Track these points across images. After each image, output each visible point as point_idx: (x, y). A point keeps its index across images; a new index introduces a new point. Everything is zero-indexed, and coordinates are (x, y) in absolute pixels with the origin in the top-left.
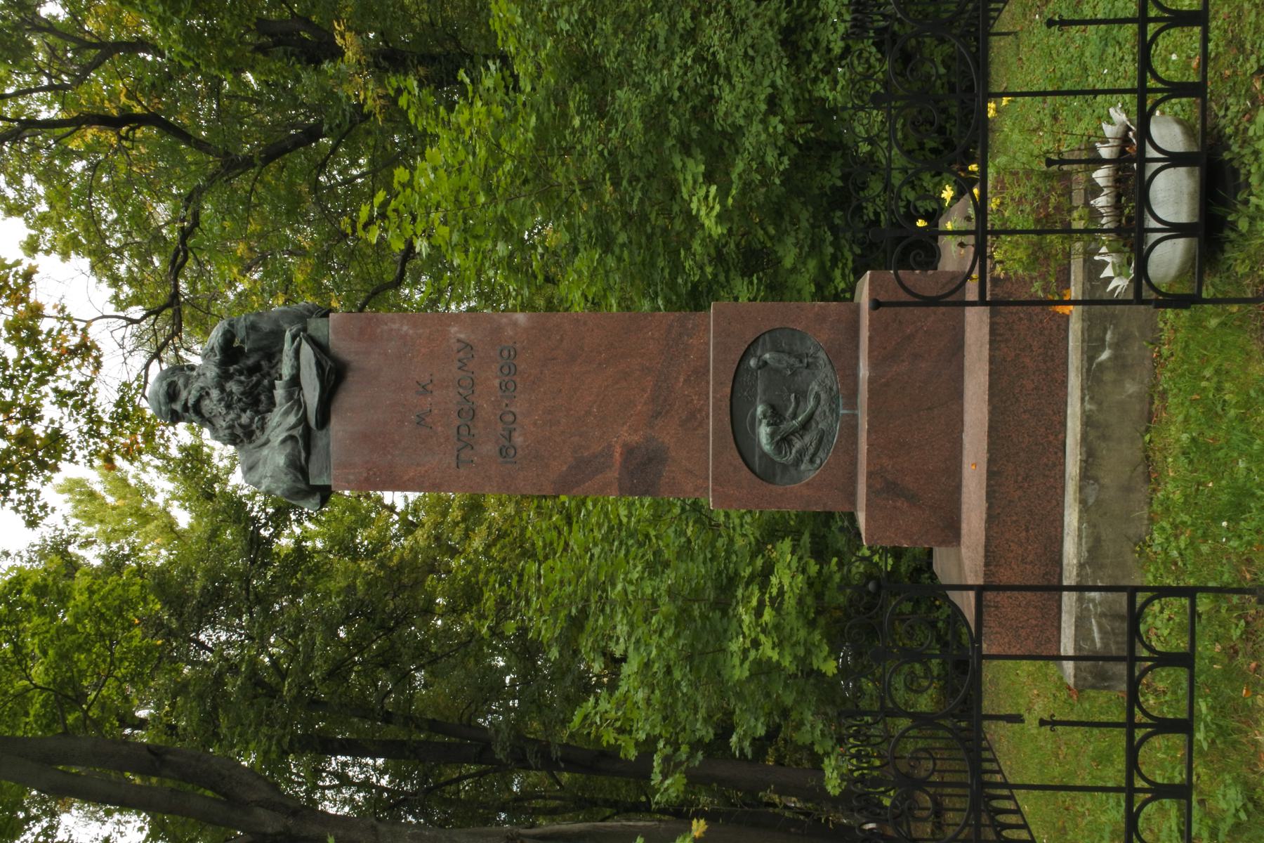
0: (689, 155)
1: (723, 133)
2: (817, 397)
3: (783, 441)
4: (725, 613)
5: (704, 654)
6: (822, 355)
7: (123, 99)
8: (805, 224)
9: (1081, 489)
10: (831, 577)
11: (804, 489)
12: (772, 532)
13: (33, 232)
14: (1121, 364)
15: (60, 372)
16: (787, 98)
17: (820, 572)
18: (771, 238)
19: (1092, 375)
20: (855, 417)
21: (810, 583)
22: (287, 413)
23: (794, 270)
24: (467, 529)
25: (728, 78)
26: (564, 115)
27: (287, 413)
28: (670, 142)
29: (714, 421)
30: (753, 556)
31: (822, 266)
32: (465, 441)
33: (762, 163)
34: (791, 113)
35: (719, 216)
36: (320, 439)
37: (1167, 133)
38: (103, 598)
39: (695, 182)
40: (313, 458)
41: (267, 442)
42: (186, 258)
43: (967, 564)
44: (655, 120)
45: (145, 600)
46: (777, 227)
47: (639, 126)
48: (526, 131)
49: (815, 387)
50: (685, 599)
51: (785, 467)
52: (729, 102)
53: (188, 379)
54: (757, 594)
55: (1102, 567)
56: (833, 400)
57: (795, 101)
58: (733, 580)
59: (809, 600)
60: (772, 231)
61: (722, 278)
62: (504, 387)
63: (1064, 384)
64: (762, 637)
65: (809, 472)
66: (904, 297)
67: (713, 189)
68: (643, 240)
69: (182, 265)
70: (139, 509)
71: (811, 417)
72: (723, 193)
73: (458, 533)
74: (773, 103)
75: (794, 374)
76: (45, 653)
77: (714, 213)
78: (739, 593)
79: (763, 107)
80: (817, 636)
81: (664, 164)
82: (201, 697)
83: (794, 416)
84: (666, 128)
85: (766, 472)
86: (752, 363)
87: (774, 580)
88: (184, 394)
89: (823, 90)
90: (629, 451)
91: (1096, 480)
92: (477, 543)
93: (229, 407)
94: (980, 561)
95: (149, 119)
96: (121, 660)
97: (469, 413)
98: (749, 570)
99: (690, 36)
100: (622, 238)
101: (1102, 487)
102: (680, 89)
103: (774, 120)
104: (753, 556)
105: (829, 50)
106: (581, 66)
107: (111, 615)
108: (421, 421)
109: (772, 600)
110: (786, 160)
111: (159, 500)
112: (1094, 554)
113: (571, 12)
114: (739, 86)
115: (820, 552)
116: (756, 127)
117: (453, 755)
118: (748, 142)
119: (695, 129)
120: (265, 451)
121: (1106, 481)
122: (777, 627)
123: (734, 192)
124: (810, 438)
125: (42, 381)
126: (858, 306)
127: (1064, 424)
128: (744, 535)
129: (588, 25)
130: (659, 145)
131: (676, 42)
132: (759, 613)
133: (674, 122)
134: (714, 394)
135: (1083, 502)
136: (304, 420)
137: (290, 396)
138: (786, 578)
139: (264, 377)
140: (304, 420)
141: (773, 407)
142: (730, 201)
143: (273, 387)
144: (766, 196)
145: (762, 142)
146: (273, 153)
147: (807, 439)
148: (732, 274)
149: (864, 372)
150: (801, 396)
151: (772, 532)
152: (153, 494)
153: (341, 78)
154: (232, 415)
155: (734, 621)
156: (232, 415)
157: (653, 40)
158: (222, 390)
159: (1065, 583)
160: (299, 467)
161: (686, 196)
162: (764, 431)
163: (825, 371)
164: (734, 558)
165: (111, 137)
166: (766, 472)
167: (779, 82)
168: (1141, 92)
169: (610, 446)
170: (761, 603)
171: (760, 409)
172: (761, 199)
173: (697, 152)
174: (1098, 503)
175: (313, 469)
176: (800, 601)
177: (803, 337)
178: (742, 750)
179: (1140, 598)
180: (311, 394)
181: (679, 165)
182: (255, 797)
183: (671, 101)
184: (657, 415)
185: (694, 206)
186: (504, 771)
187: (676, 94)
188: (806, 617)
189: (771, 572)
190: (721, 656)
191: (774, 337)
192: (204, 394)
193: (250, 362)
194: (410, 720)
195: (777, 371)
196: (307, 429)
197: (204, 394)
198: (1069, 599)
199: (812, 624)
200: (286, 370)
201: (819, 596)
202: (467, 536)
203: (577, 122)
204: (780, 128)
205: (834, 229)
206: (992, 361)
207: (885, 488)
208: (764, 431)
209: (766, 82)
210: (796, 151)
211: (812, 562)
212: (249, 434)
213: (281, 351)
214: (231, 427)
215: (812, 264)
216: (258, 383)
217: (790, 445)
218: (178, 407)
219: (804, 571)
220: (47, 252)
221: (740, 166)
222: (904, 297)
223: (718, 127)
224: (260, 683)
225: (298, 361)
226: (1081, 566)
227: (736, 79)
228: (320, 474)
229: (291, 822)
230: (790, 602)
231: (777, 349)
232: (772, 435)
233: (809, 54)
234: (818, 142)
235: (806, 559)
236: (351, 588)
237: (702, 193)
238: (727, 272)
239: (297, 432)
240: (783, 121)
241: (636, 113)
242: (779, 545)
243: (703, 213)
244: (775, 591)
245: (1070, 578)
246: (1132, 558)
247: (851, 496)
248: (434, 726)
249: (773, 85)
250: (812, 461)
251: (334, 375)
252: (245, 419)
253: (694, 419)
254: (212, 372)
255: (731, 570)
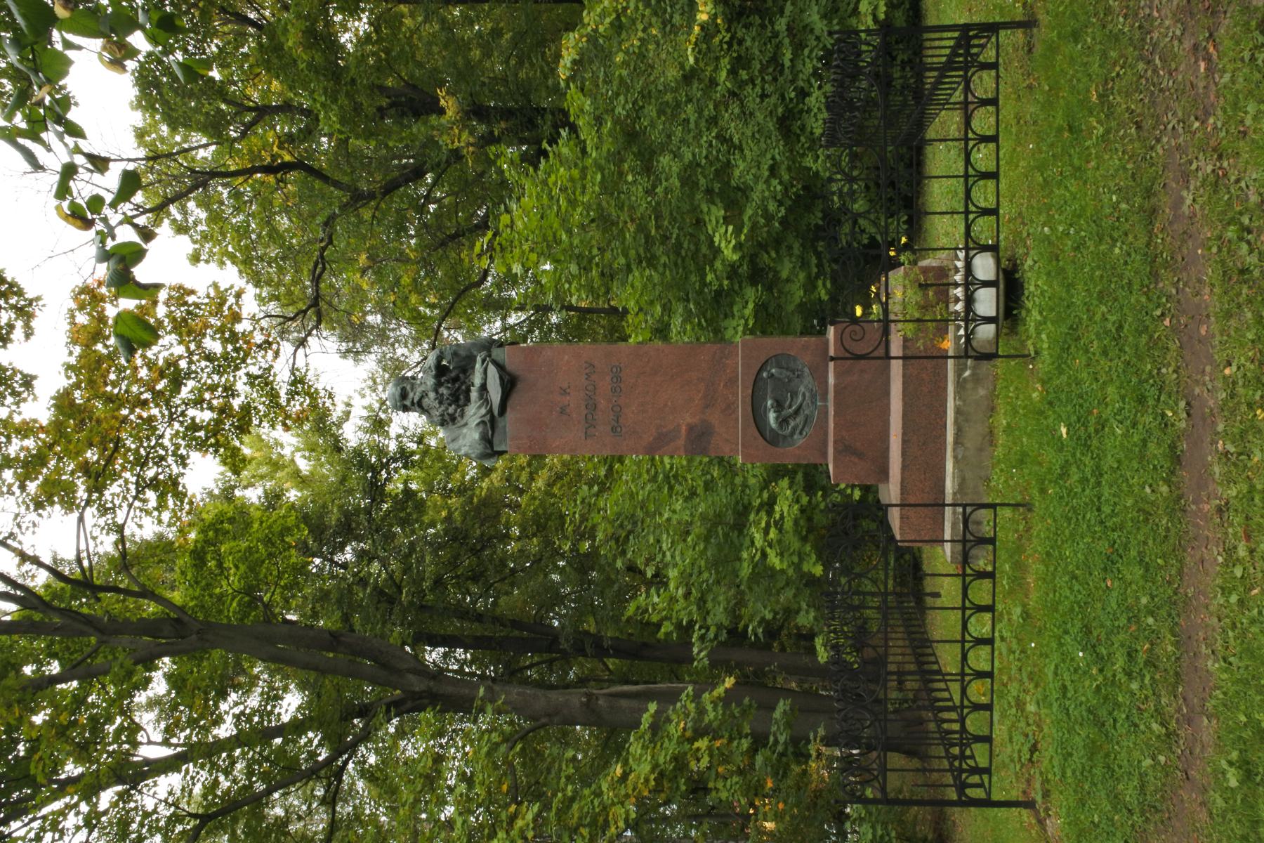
0: (713, 203)
1: (738, 188)
2: (804, 395)
3: (783, 422)
4: (741, 532)
5: (725, 560)
6: (806, 370)
7: (275, 149)
8: (796, 251)
9: (954, 450)
10: (818, 505)
11: (796, 450)
12: (776, 473)
13: (197, 246)
14: (976, 378)
15: (249, 361)
16: (783, 167)
17: (810, 502)
18: (773, 260)
19: (960, 385)
20: (826, 407)
21: (802, 511)
22: (480, 407)
23: (788, 280)
24: (531, 473)
25: (742, 150)
26: (621, 174)
27: (480, 407)
28: (699, 196)
29: (741, 409)
30: (761, 490)
31: (809, 277)
32: (590, 423)
33: (766, 210)
34: (786, 177)
35: (735, 248)
36: (501, 423)
37: (984, 266)
38: (270, 527)
39: (717, 222)
40: (496, 435)
41: (466, 424)
42: (324, 269)
43: (892, 493)
44: (688, 180)
45: (298, 527)
46: (777, 253)
47: (677, 183)
48: (594, 185)
49: (802, 389)
50: (714, 521)
51: (785, 437)
52: (740, 169)
53: (413, 385)
54: (765, 518)
55: (966, 494)
56: (813, 396)
57: (789, 169)
58: (747, 509)
59: (802, 522)
60: (773, 255)
61: (736, 287)
62: (614, 390)
63: (945, 389)
64: (768, 550)
65: (799, 440)
66: (847, 355)
67: (731, 228)
68: (679, 261)
69: (320, 275)
70: (271, 458)
71: (800, 406)
72: (738, 231)
73: (524, 477)
74: (773, 170)
75: (790, 381)
76: (237, 567)
77: (731, 245)
78: (752, 517)
79: (767, 174)
80: (808, 548)
81: (695, 209)
82: (339, 602)
83: (790, 406)
84: (696, 184)
85: (773, 439)
86: (765, 375)
87: (777, 508)
88: (411, 395)
89: (808, 162)
90: (691, 428)
91: (963, 445)
92: (540, 483)
93: (441, 403)
94: (899, 492)
95: (297, 165)
96: (284, 573)
97: (592, 406)
98: (759, 501)
99: (713, 121)
100: (664, 259)
101: (966, 449)
102: (706, 157)
103: (775, 182)
104: (761, 490)
105: (812, 133)
106: (631, 135)
107: (275, 539)
108: (563, 411)
109: (776, 523)
110: (783, 210)
111: (287, 452)
112: (961, 487)
113: (626, 102)
114: (749, 157)
115: (810, 488)
116: (761, 186)
117: (524, 646)
118: (756, 196)
119: (717, 186)
120: (465, 430)
121: (968, 445)
122: (779, 542)
123: (745, 231)
124: (800, 419)
125: (237, 368)
126: (827, 341)
127: (945, 412)
128: (755, 476)
129: (638, 111)
130: (691, 197)
131: (703, 124)
132: (766, 532)
133: (702, 181)
134: (742, 395)
135: (955, 457)
136: (490, 411)
137: (481, 397)
138: (785, 507)
139: (462, 384)
140: (490, 411)
141: (777, 401)
142: (743, 237)
143: (468, 391)
144: (768, 232)
145: (765, 195)
146: (390, 188)
147: (798, 420)
148: (744, 284)
149: (831, 380)
150: (794, 394)
151: (776, 473)
152: (282, 447)
153: (442, 130)
154: (443, 408)
155: (748, 539)
156: (443, 408)
157: (687, 121)
158: (437, 392)
159: (900, 361)
160: (487, 440)
161: (710, 232)
162: (772, 416)
163: (808, 379)
164: (748, 491)
165: (271, 179)
166: (773, 439)
167: (777, 157)
168: (967, 249)
169: (679, 425)
170: (768, 524)
171: (769, 403)
172: (765, 235)
173: (718, 200)
174: (964, 457)
175: (496, 441)
176: (796, 522)
177: (795, 359)
178: (756, 635)
179: (969, 510)
180: (495, 394)
181: (705, 209)
182: (406, 666)
183: (698, 165)
184: (707, 406)
185: (716, 239)
186: (566, 659)
187: (704, 161)
188: (800, 534)
189: (775, 503)
190: (738, 563)
191: (779, 359)
192: (424, 395)
193: (453, 375)
194: (497, 620)
195: (779, 379)
196: (493, 416)
197: (424, 395)
198: (948, 510)
199: (804, 539)
200: (477, 380)
201: (810, 519)
202: (532, 478)
203: (630, 178)
204: (779, 188)
205: (819, 255)
206: (904, 376)
207: (844, 449)
208: (772, 416)
209: (769, 156)
210: (790, 203)
211: (804, 495)
212: (453, 419)
213: (473, 368)
214: (442, 415)
215: (802, 276)
216: (459, 388)
217: (788, 424)
218: (408, 403)
219: (798, 501)
220: (207, 262)
221: (749, 212)
222: (847, 355)
223: (733, 183)
224: (382, 593)
225: (485, 376)
226: (954, 494)
227: (747, 152)
228: (500, 443)
229: (432, 683)
230: (788, 524)
231: (779, 366)
232: (777, 418)
233: (798, 136)
234: (809, 193)
235: (799, 492)
236: (449, 519)
237: (723, 230)
238: (740, 283)
239: (487, 419)
240: (781, 183)
241: (675, 175)
242: (780, 482)
243: (723, 245)
244: (777, 516)
245: (949, 499)
246: (982, 489)
247: (825, 455)
248: (516, 624)
249: (773, 158)
250: (801, 433)
251: (509, 384)
252: (451, 410)
253: (729, 408)
254: (431, 382)
255: (746, 501)
